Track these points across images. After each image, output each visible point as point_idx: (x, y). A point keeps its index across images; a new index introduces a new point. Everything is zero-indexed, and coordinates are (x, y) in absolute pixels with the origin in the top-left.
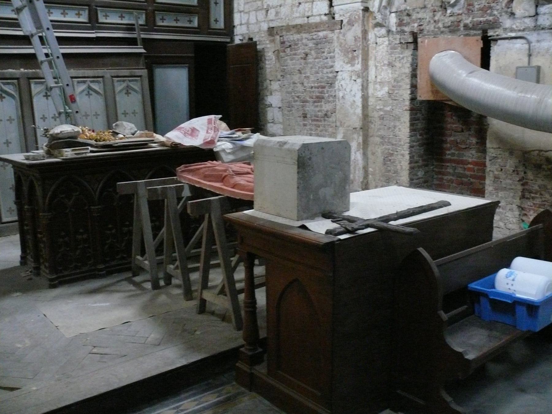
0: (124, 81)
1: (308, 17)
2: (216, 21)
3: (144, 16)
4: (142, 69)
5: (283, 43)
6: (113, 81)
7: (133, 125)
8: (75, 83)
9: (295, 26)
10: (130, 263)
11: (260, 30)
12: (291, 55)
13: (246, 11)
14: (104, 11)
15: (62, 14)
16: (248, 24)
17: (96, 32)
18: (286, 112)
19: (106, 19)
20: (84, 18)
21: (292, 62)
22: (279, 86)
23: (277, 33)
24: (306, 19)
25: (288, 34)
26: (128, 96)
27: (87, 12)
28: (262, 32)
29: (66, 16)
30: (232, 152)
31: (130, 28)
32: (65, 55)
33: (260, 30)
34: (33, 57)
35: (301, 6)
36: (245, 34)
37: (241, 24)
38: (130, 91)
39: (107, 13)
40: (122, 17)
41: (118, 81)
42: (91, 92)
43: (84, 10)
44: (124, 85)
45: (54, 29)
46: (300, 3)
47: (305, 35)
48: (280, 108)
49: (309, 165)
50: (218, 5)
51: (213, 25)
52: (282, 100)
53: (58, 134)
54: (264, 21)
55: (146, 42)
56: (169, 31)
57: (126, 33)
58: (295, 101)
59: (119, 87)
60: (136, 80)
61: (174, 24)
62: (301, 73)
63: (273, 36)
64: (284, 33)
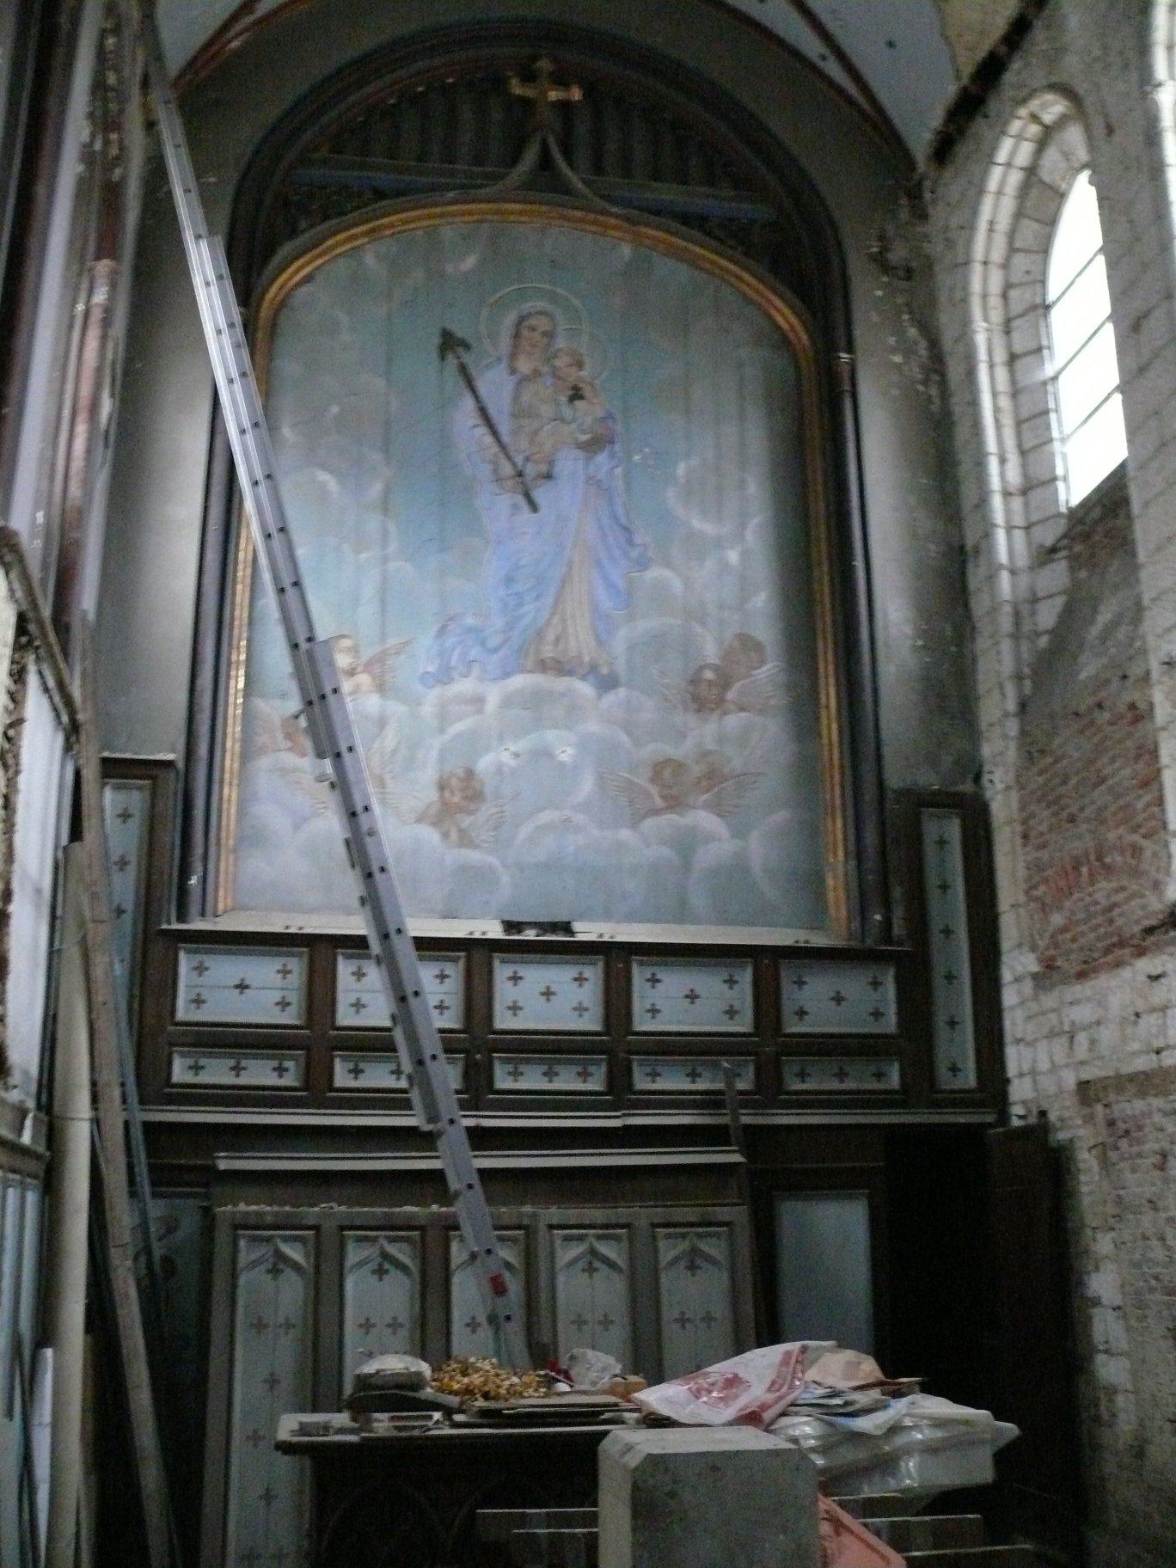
0: (684, 1236)
1: (1158, 1053)
2: (954, 1069)
3: (751, 1069)
4: (738, 1205)
5: (1111, 1123)
6: (654, 1238)
7: (611, 1360)
8: (558, 1242)
9: (1132, 1078)
11: (1060, 1087)
12: (1131, 1157)
13: (1029, 1038)
15: (545, 1074)
16: (1033, 1072)
17: (624, 1115)
18: (1133, 1322)
20: (596, 1083)
21: (1135, 1176)
22: (1112, 1246)
23: (1096, 1095)
24: (1154, 1056)
25: (1120, 1098)
26: (693, 1275)
28: (1066, 1096)
30: (820, 1446)
31: (711, 1101)
32: (484, 1174)
33: (1060, 1087)
34: (438, 1177)
35: (1143, 1021)
36: (1031, 1101)
37: (1021, 1075)
38: (699, 1262)
40: (694, 1075)
41: (668, 1236)
42: (597, 1264)
43: (597, 1063)
44: (684, 1245)
46: (1137, 1015)
47: (1157, 1102)
48: (1119, 1308)
49: (671, 1513)
50: (957, 1027)
51: (947, 1081)
52: (1122, 1286)
53: (371, 1376)
54: (1067, 1065)
55: (754, 1139)
56: (821, 1104)
58: (1152, 1290)
59: (668, 1250)
60: (718, 1235)
61: (835, 1085)
62: (1156, 1209)
63: (1090, 1106)
64: (1112, 1097)
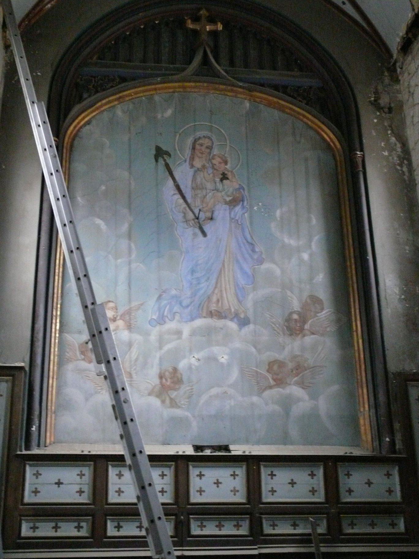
3: (325, 522)
10: (173, 61)
14: (278, 519)
19: (274, 529)
20: (244, 531)
27: (248, 522)
29: (222, 528)
39: (275, 521)
40: (295, 525)
43: (243, 519)
45: (174, 547)
57: (301, 547)
61: (369, 530)
